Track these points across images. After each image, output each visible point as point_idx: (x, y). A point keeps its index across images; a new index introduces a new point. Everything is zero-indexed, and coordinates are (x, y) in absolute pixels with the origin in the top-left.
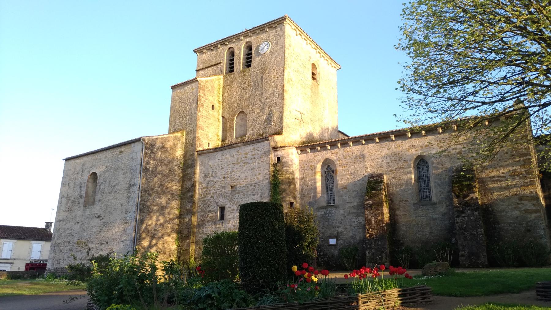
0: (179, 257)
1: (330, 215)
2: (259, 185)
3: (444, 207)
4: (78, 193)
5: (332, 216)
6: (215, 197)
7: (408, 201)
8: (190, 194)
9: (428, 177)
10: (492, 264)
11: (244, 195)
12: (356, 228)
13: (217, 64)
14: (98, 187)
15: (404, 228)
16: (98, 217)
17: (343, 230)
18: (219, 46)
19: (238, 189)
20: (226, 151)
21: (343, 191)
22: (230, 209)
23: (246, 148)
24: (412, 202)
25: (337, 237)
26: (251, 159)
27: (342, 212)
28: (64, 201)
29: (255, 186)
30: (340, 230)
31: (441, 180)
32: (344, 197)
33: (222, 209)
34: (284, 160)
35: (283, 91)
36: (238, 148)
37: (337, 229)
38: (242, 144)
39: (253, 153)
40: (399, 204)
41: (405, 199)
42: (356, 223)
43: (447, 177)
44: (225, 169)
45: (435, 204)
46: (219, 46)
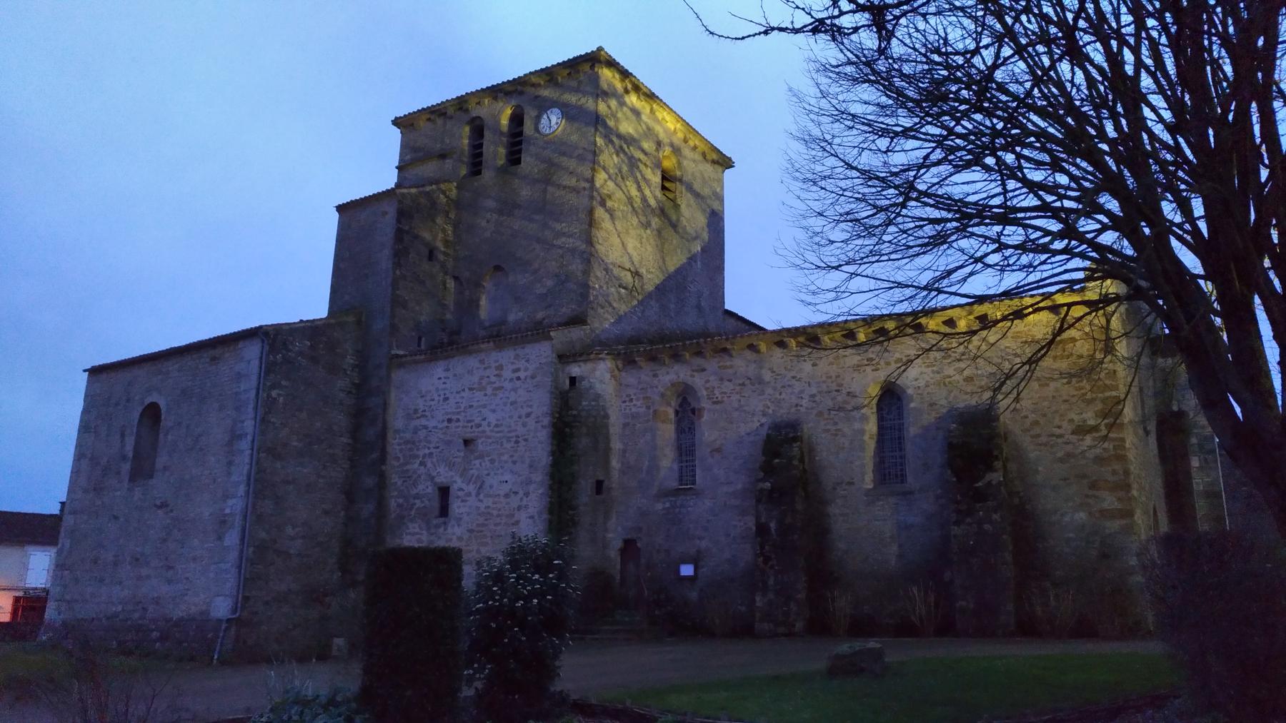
2: (526, 440)
6: (429, 465)
7: (852, 483)
11: (492, 461)
14: (161, 436)
16: (160, 507)
19: (480, 447)
22: (460, 493)
25: (695, 561)
26: (511, 380)
27: (708, 503)
28: (85, 463)
29: (517, 442)
30: (704, 544)
33: (444, 492)
36: (482, 356)
39: (515, 367)
40: (835, 489)
44: (452, 401)
45: (911, 493)
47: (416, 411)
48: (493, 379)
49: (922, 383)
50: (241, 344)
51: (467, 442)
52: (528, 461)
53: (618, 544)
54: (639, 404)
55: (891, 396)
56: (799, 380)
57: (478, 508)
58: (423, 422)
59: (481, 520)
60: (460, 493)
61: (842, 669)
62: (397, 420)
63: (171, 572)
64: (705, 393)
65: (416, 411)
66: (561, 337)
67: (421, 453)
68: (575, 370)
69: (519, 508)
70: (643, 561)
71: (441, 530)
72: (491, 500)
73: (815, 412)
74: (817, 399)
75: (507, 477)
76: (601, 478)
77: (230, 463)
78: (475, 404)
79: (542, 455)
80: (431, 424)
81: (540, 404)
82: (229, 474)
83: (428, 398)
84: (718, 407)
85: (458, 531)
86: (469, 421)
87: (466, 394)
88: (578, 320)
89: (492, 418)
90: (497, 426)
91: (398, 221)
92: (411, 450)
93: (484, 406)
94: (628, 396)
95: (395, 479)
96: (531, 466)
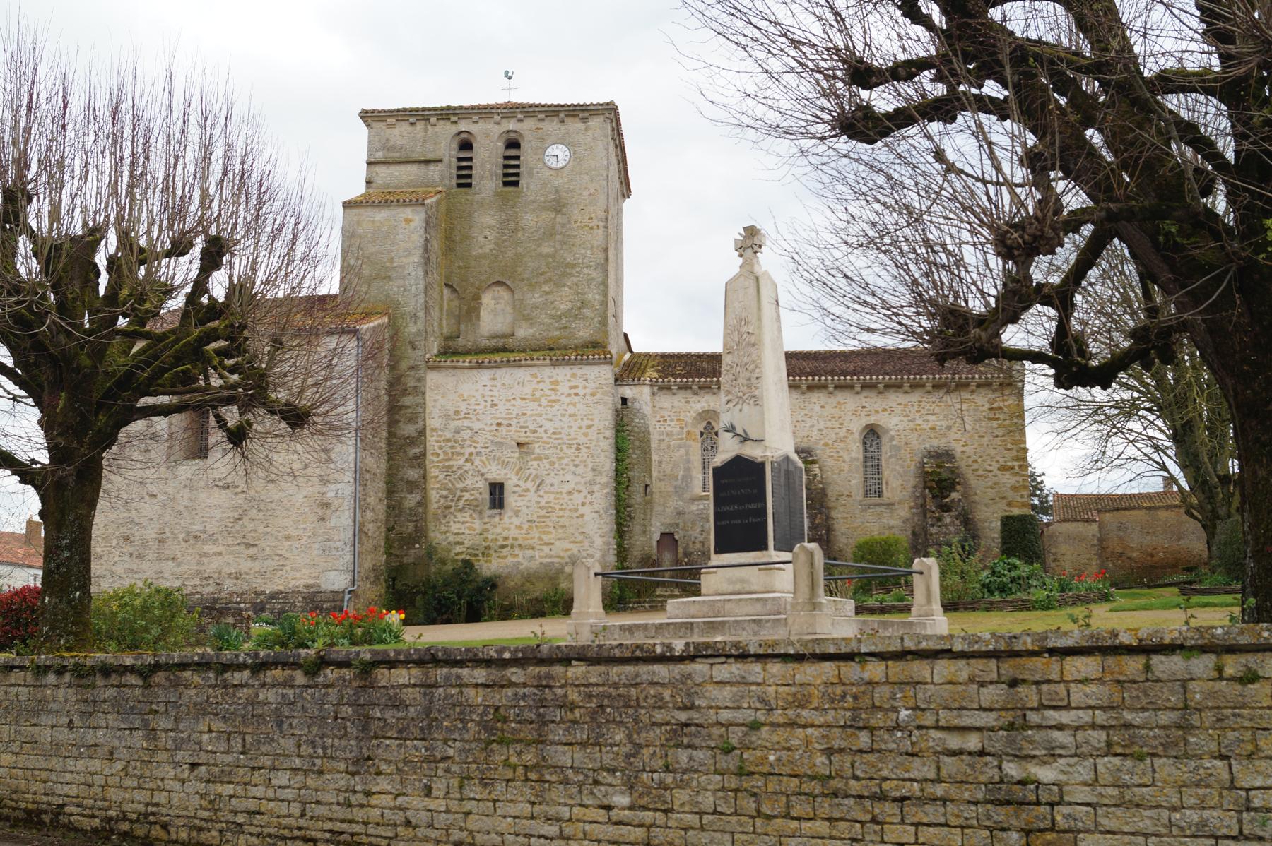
0: (394, 580)
6: (477, 462)
8: (417, 451)
10: (692, 624)
11: (552, 464)
13: (427, 162)
16: (226, 487)
18: (433, 120)
19: (537, 451)
22: (517, 489)
26: (569, 395)
29: (578, 449)
31: (902, 466)
36: (534, 370)
44: (502, 408)
46: (433, 120)
47: (457, 413)
52: (591, 465)
53: (657, 536)
57: (538, 502)
58: (466, 423)
59: (543, 512)
65: (457, 413)
67: (468, 451)
69: (583, 504)
71: (497, 519)
72: (552, 496)
78: (529, 413)
80: (477, 426)
81: (603, 418)
85: (516, 521)
92: (452, 447)
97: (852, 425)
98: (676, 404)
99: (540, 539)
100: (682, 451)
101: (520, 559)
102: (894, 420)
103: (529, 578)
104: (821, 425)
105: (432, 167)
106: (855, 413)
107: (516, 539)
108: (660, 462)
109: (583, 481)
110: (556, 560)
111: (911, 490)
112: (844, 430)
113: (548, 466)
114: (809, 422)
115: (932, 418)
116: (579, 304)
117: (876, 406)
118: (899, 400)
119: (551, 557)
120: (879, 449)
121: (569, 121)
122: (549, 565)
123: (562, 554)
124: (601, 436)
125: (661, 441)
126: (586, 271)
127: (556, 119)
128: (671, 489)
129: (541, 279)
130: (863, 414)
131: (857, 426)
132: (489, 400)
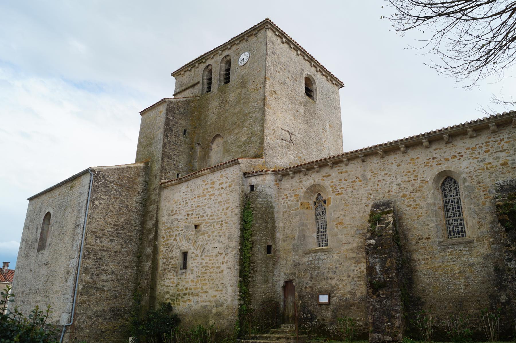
1: (320, 262)
2: (226, 223)
3: (486, 246)
4: (34, 236)
5: (323, 263)
6: (178, 240)
7: (430, 239)
9: (458, 202)
11: (209, 236)
12: (355, 279)
14: (50, 228)
15: (425, 280)
17: (338, 283)
19: (203, 229)
20: (192, 181)
21: (337, 227)
22: (193, 255)
23: (213, 176)
24: (437, 240)
26: (219, 189)
27: (336, 257)
30: (334, 282)
32: (339, 236)
33: (185, 255)
34: (259, 189)
35: (264, 105)
36: (204, 178)
37: (329, 281)
38: (208, 170)
39: (220, 182)
40: (417, 243)
41: (425, 236)
42: (356, 272)
43: (488, 200)
44: (189, 204)
45: (471, 242)
46: (197, 65)
48: (210, 190)
49: (471, 169)
50: (82, 177)
51: (196, 226)
52: (227, 234)
53: (282, 283)
54: (292, 199)
55: (447, 181)
56: (389, 176)
57: (202, 263)
58: (176, 217)
60: (193, 255)
61: (36, 240)
62: (164, 218)
63: (47, 299)
64: (331, 189)
66: (245, 164)
68: (253, 181)
70: (297, 294)
71: (184, 276)
72: (208, 258)
73: (401, 194)
74: (402, 186)
75: (217, 245)
76: (270, 244)
77: (73, 240)
78: (200, 205)
79: (236, 233)
80: (179, 217)
81: (234, 201)
82: (73, 246)
83: (178, 203)
84: (339, 196)
85: (191, 277)
86: (197, 215)
87: (196, 199)
88: (259, 156)
89: (209, 212)
90: (211, 216)
91: (167, 114)
92: (170, 232)
93: (205, 206)
94: (286, 195)
95: (162, 248)
96: (229, 238)
97: (425, 175)
98: (294, 184)
99: (202, 289)
100: (298, 218)
101: (192, 303)
102: (464, 164)
103: (196, 315)
104: (399, 180)
105: (196, 87)
106: (427, 165)
107: (191, 289)
108: (284, 228)
109: (223, 246)
110: (208, 304)
111: (488, 226)
112: (419, 181)
113: (207, 238)
114: (389, 179)
115: (502, 155)
116: (250, 135)
117: (446, 155)
118: (467, 146)
119: (206, 302)
120: (457, 193)
121: (249, 39)
122: (205, 307)
123: (212, 299)
124: (233, 213)
125: (285, 212)
126: (254, 115)
127: (244, 41)
128: (290, 247)
129: (235, 126)
130: (434, 164)
131: (430, 175)
132: (184, 200)
